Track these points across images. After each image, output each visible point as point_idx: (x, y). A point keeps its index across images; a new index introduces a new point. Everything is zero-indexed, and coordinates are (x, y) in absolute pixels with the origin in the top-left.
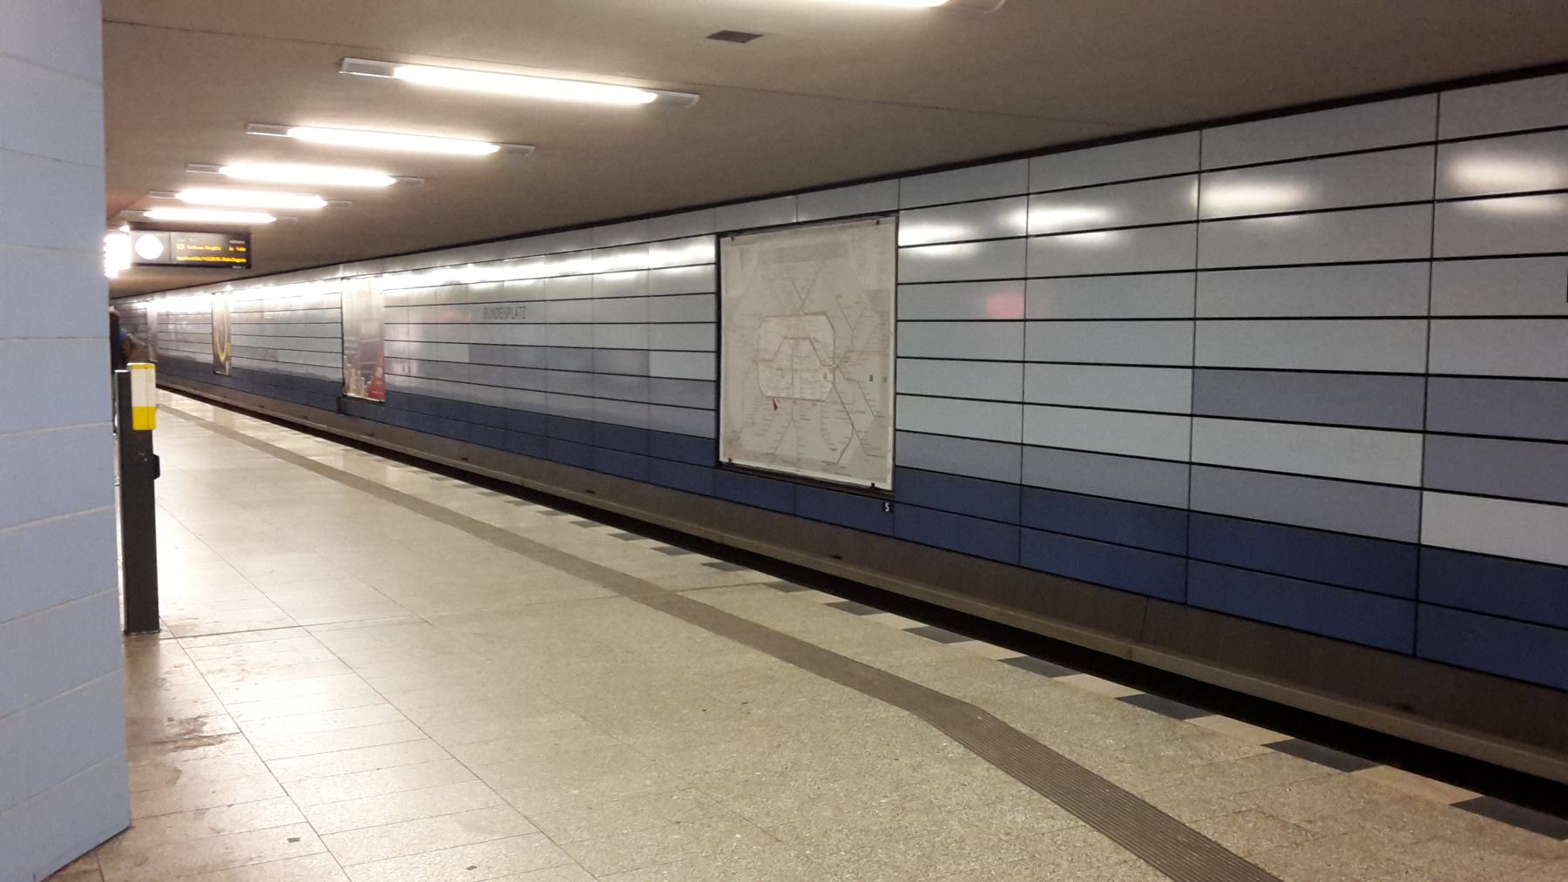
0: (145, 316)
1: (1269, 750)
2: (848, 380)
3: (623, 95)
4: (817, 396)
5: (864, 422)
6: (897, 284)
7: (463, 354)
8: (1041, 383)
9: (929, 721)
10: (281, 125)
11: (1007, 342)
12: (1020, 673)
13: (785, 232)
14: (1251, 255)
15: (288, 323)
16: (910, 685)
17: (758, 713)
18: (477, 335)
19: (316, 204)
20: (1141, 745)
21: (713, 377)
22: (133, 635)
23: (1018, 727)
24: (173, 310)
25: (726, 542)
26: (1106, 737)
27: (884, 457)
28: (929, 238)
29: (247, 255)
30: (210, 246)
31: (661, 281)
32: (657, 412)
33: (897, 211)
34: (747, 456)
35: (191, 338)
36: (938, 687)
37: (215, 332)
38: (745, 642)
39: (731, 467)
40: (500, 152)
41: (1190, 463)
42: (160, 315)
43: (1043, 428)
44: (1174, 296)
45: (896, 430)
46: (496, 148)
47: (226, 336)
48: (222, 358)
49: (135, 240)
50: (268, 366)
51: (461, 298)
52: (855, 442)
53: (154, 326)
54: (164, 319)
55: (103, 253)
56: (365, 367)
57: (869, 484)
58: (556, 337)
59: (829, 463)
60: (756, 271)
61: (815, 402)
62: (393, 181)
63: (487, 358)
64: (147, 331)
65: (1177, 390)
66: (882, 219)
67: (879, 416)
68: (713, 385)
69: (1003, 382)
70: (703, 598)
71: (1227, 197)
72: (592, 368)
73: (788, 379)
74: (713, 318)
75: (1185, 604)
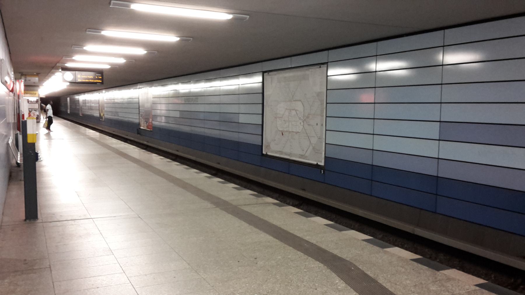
0: (79, 101)
1: (477, 288)
2: (309, 125)
3: (221, 16)
4: (298, 130)
5: (314, 140)
6: (327, 90)
7: (177, 114)
8: (381, 127)
9: (331, 269)
10: (99, 30)
11: (367, 111)
12: (371, 247)
13: (287, 71)
14: (462, 80)
15: (122, 103)
16: (325, 251)
17: (261, 263)
18: (182, 108)
19: (122, 61)
20: (421, 283)
21: (261, 123)
22: (28, 221)
23: (369, 273)
24: (87, 99)
25: (264, 183)
26: (406, 279)
27: (321, 153)
28: (340, 74)
29: (102, 79)
30: (89, 76)
31: (243, 89)
32: (241, 135)
33: (327, 63)
34: (272, 152)
35: (93, 108)
36: (336, 252)
37: (100, 106)
38: (260, 229)
39: (267, 155)
40: (180, 40)
41: (438, 158)
42: (83, 100)
43: (381, 144)
44: (433, 94)
45: (326, 144)
46: (178, 39)
47: (103, 108)
48: (102, 115)
49: (63, 74)
50: (115, 118)
51: (177, 95)
52: (311, 148)
53: (81, 104)
54: (85, 102)
55: (50, 76)
56: (146, 119)
57: (315, 163)
58: (207, 108)
59: (302, 155)
60: (277, 85)
61: (297, 133)
62: (146, 52)
63: (187, 116)
64: (79, 106)
65: (434, 130)
66: (322, 66)
67: (320, 138)
68: (261, 126)
69: (366, 126)
70: (247, 209)
71: (451, 58)
72: (226, 120)
73: (287, 124)
74: (261, 102)
75: (435, 212)
